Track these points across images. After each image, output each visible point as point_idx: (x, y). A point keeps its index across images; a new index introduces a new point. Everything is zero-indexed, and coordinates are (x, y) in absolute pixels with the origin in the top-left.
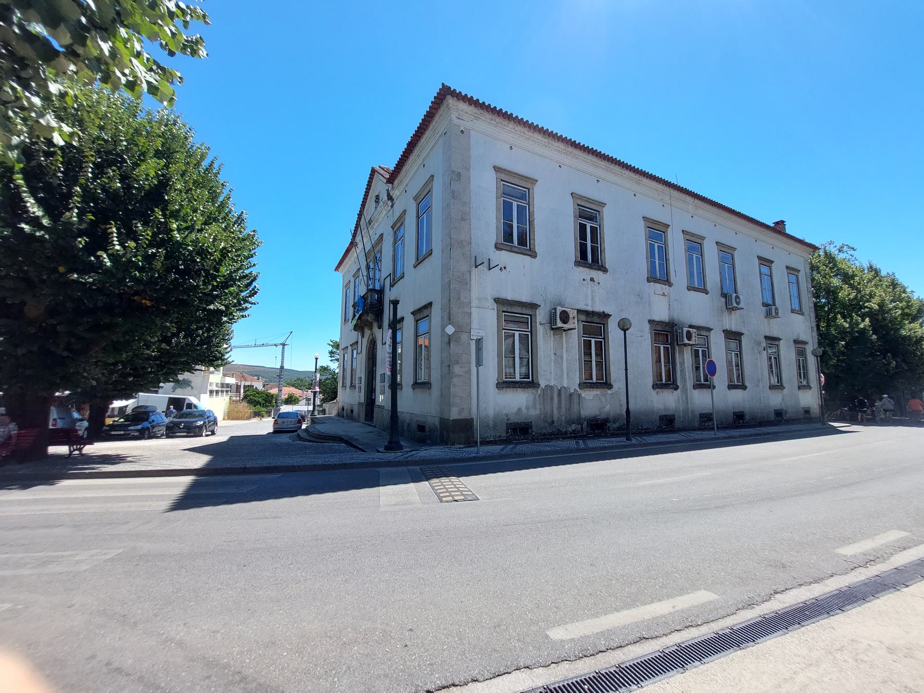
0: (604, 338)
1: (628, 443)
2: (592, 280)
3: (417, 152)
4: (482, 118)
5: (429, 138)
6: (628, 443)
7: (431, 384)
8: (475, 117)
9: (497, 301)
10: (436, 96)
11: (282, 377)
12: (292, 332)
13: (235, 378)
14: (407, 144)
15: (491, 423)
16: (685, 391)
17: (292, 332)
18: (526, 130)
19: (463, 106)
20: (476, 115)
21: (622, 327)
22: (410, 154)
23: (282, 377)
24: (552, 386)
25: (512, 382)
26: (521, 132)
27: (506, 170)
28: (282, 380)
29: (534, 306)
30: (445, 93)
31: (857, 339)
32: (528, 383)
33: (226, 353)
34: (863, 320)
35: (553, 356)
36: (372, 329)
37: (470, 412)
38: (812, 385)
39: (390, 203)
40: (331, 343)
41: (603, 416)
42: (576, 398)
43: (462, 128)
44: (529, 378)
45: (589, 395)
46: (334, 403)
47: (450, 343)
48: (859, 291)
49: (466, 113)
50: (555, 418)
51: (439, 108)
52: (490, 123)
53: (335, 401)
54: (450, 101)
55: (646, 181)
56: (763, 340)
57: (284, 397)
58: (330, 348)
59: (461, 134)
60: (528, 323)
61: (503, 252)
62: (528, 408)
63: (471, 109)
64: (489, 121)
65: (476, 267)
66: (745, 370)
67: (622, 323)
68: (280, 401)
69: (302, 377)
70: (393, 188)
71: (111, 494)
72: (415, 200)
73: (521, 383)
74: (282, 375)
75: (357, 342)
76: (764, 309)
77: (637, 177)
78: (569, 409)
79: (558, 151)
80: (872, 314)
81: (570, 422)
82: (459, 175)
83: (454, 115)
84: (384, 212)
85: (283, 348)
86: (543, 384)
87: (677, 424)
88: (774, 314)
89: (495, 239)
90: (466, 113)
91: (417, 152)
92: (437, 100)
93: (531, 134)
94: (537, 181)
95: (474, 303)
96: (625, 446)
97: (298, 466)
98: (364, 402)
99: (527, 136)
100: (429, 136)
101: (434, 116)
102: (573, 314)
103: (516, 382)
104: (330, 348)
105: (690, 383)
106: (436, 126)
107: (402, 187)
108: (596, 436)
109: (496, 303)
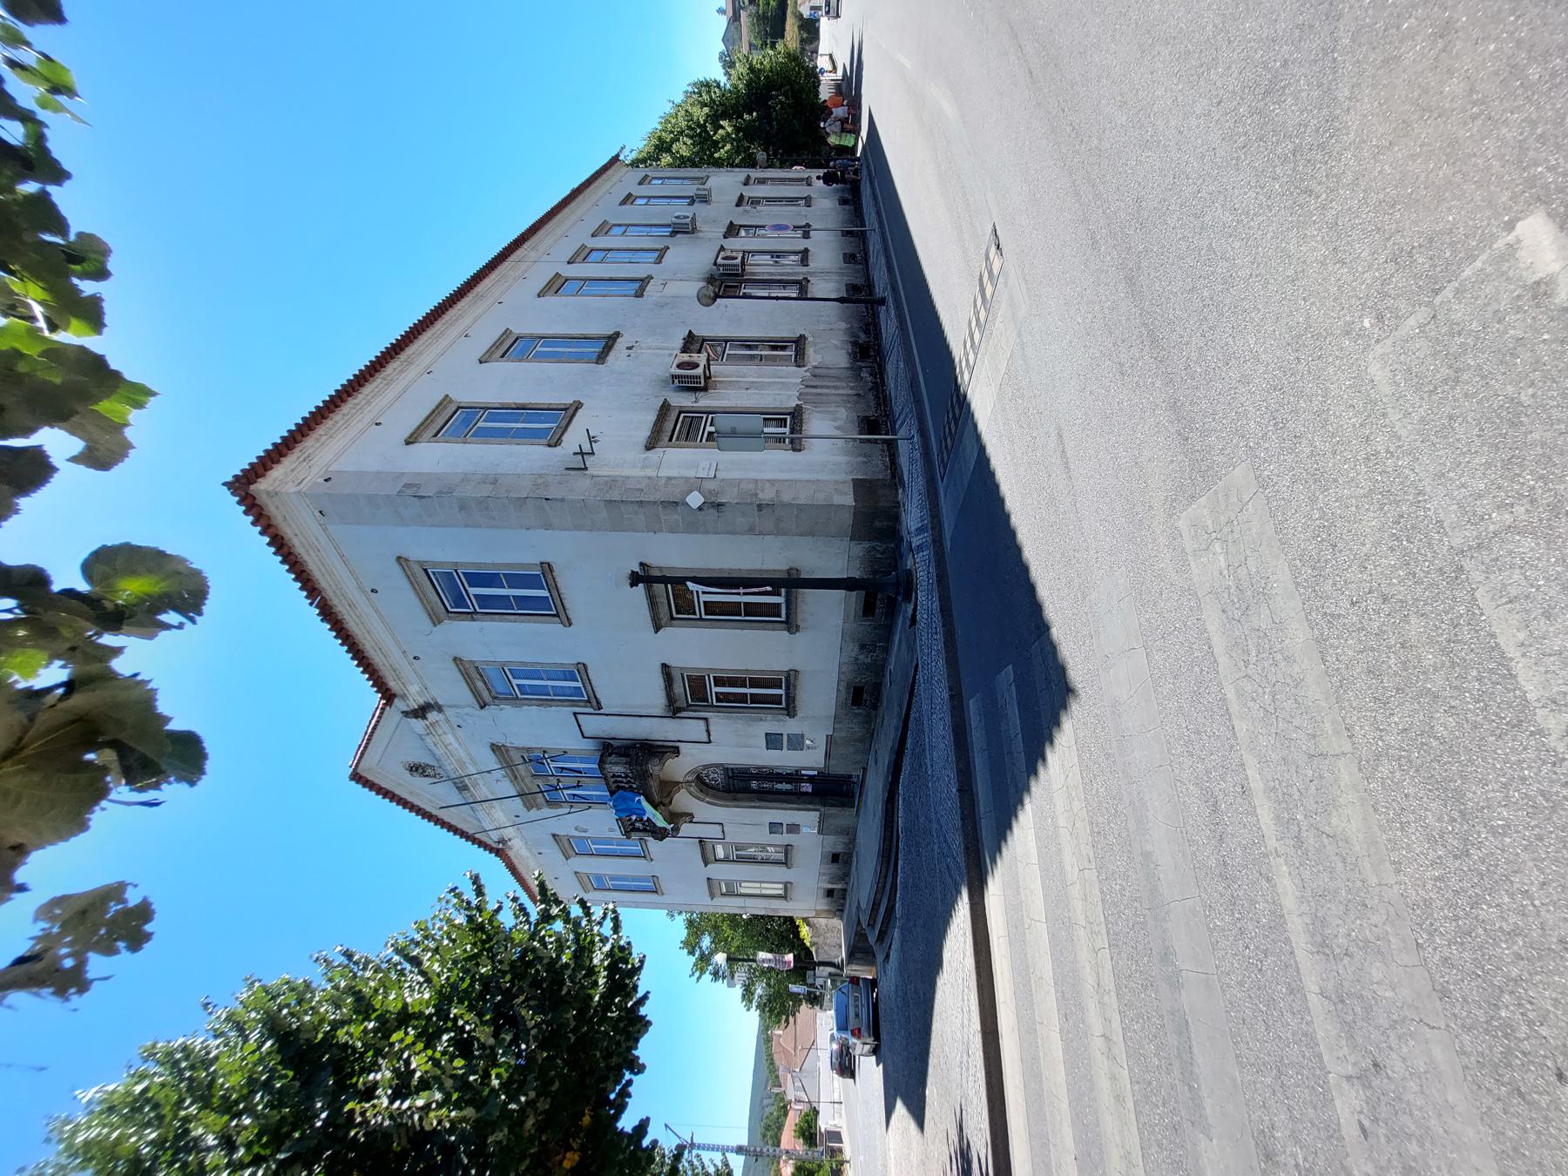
0: (726, 342)
1: (890, 301)
2: (630, 348)
3: (343, 606)
4: (310, 451)
5: (323, 564)
6: (890, 301)
7: (790, 569)
8: (304, 460)
9: (650, 445)
10: (237, 499)
11: (758, 1150)
12: (666, 1126)
13: (761, 1007)
14: (322, 620)
15: (861, 459)
16: (811, 274)
17: (666, 1126)
18: (351, 402)
19: (277, 472)
20: (302, 459)
21: (710, 301)
22: (343, 628)
23: (758, 1150)
24: (800, 394)
25: (788, 608)
26: (354, 408)
27: (418, 428)
28: (765, 1150)
29: (665, 408)
30: (244, 486)
31: (748, 134)
32: (795, 417)
33: (703, 1168)
34: (723, 128)
35: (749, 391)
36: (678, 783)
37: (844, 482)
38: (806, 176)
39: (433, 716)
40: (697, 974)
41: (849, 347)
42: (818, 371)
43: (321, 480)
44: (786, 419)
45: (813, 357)
46: (816, 951)
47: (720, 505)
48: (681, 133)
49: (292, 470)
50: (854, 392)
51: (269, 518)
52: (323, 444)
53: (813, 950)
54: (261, 487)
55: (481, 288)
56: (741, 208)
57: (800, 1146)
58: (707, 977)
59: (330, 483)
60: (693, 417)
61: (564, 438)
62: (835, 420)
63: (287, 463)
64: (318, 444)
65: (586, 469)
66: (777, 404)
67: (704, 301)
68: (810, 1153)
69: (760, 1130)
70: (404, 697)
71: (1048, 1003)
72: (440, 622)
73: (788, 688)
74: (755, 1151)
75: (701, 841)
76: (696, 205)
77: (471, 296)
78: (838, 378)
79: (402, 371)
80: (715, 119)
81: (858, 377)
82: (407, 486)
83: (291, 488)
84: (450, 738)
85: (699, 1147)
86: (793, 403)
87: (859, 282)
88: (706, 193)
89: (541, 447)
90: (292, 470)
91: (343, 606)
92: (246, 502)
93: (360, 397)
94: (447, 396)
95: (651, 472)
96: (898, 307)
97: (951, 689)
98: (817, 813)
99: (364, 402)
100: (318, 563)
101: (282, 538)
102: (685, 357)
103: (787, 694)
104: (707, 977)
105: (805, 269)
106: (303, 540)
107: (406, 670)
108: (879, 354)
109: (654, 448)
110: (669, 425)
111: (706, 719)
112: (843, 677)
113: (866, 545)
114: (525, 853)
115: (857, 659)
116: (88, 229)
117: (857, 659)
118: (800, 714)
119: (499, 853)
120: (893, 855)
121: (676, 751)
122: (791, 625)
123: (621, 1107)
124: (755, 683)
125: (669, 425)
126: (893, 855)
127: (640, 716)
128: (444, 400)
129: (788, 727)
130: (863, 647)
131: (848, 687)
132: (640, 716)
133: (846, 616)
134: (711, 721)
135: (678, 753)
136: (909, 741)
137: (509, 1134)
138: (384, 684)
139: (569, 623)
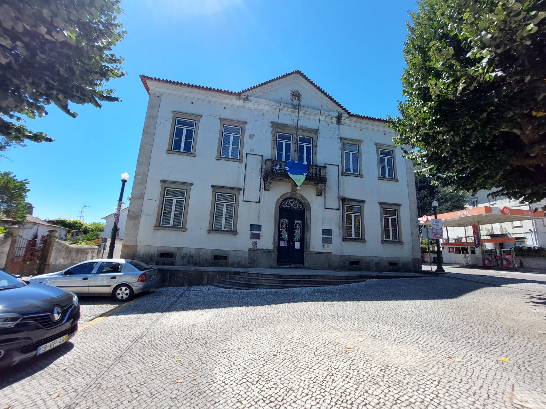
25: (389, 241)
110: (386, 206)
111: (339, 209)
112: (364, 257)
113: (411, 262)
114: (224, 101)
115: (372, 262)
116: (399, 86)
117: (372, 262)
118: (343, 243)
119: (239, 94)
120: (305, 285)
121: (319, 194)
122: (383, 242)
123: (71, 100)
124: (357, 228)
125: (386, 206)
126: (305, 285)
127: (339, 187)
128: (357, 141)
129: (336, 237)
130: (377, 263)
131: (360, 258)
132: (339, 187)
133: (389, 258)
134: (338, 211)
135: (318, 195)
136: (359, 283)
137: (528, 186)
138: (284, 77)
139: (397, 181)
